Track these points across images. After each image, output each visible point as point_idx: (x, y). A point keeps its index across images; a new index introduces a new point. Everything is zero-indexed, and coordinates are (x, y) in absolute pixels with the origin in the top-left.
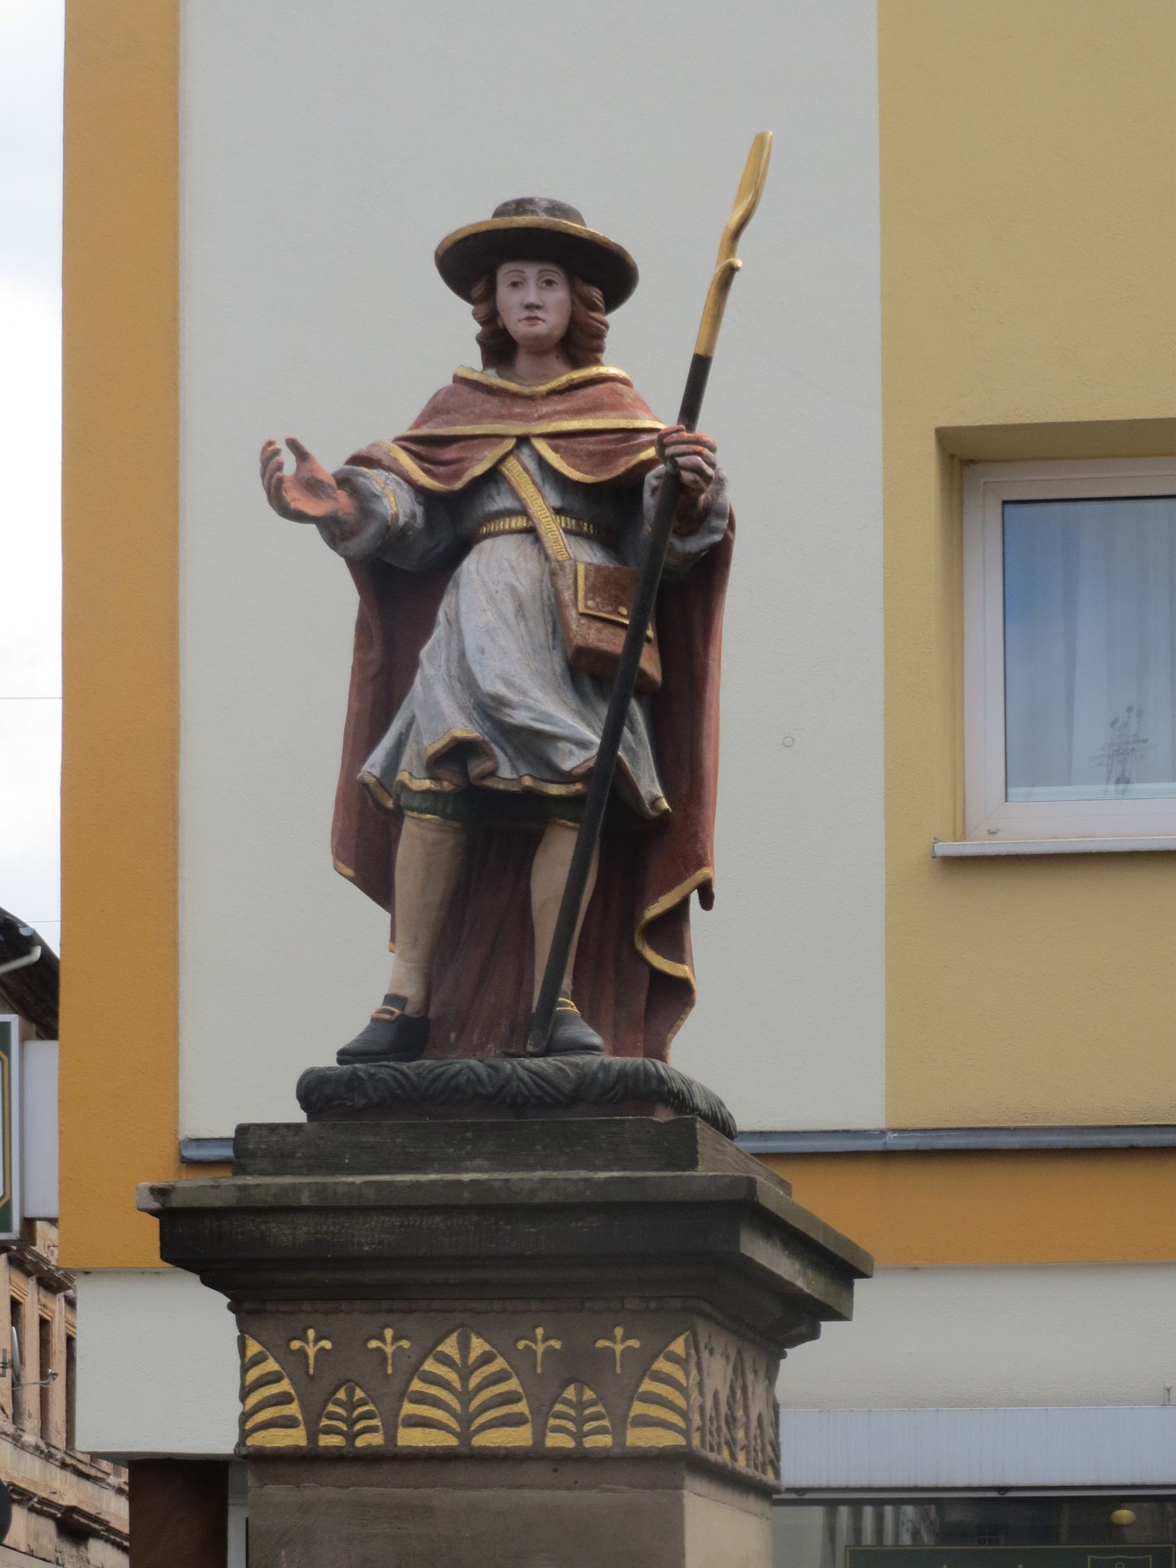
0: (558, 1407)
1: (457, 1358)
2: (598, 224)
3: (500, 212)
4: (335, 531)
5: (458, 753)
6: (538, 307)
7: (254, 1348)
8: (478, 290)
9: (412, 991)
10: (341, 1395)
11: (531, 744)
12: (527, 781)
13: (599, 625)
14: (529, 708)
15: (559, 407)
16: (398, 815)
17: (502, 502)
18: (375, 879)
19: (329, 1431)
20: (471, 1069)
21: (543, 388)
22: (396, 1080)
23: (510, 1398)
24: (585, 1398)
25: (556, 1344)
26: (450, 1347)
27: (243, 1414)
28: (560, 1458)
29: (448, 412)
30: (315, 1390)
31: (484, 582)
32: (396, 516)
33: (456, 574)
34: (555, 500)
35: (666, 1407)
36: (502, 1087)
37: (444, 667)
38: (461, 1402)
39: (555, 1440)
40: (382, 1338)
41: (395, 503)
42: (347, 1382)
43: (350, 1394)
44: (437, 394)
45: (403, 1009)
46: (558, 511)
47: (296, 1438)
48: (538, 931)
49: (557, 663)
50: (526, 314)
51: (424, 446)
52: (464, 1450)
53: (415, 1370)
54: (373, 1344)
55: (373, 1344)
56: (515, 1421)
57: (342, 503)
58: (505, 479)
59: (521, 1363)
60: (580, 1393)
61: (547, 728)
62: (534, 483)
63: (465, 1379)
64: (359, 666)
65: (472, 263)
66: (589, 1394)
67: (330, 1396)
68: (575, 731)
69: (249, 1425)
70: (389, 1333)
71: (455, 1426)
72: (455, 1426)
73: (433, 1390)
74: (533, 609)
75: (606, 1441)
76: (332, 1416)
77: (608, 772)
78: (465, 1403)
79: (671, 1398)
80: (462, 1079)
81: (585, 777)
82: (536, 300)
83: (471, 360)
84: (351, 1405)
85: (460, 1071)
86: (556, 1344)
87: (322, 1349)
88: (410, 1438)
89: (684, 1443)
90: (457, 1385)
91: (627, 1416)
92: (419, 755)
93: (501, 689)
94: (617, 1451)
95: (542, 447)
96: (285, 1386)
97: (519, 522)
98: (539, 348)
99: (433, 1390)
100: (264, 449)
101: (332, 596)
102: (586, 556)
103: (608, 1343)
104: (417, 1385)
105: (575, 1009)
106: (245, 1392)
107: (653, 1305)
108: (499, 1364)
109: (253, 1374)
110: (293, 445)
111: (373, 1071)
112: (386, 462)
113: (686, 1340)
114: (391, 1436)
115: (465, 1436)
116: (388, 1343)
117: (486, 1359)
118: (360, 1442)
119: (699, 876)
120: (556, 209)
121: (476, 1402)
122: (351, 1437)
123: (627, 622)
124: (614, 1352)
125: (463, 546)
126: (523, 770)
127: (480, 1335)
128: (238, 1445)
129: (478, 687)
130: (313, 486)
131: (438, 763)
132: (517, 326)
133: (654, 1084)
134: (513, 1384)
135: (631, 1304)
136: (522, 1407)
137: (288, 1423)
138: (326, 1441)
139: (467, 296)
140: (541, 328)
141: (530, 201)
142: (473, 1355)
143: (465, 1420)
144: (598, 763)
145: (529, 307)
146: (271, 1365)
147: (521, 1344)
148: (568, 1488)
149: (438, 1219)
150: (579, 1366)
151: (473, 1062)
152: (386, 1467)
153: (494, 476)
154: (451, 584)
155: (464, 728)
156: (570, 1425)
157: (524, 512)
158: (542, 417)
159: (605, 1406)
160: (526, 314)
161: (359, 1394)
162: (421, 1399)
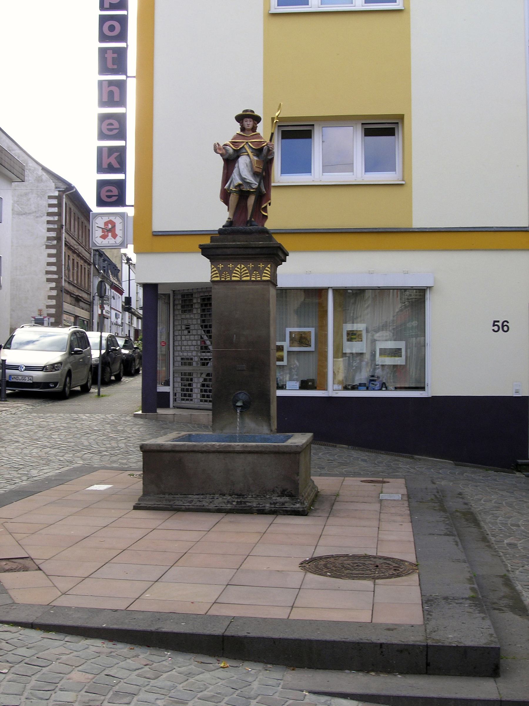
3: (244, 111)
4: (222, 155)
5: (240, 185)
7: (213, 267)
9: (231, 217)
11: (249, 184)
16: (230, 193)
17: (244, 151)
23: (247, 273)
26: (239, 266)
28: (253, 281)
39: (253, 279)
41: (231, 151)
42: (226, 271)
47: (218, 279)
49: (252, 173)
56: (248, 276)
59: (248, 268)
64: (224, 173)
65: (240, 118)
68: (254, 182)
74: (249, 165)
75: (259, 279)
77: (259, 189)
82: (249, 123)
83: (239, 131)
84: (225, 274)
88: (234, 279)
93: (245, 177)
95: (249, 143)
96: (217, 272)
97: (246, 154)
98: (249, 130)
101: (220, 163)
102: (256, 158)
104: (234, 272)
106: (212, 272)
108: (245, 268)
110: (218, 143)
114: (231, 279)
116: (231, 266)
117: (244, 268)
122: (226, 279)
125: (238, 157)
130: (220, 149)
131: (236, 187)
132: (246, 127)
137: (217, 277)
143: (241, 276)
146: (215, 269)
150: (256, 269)
153: (243, 147)
155: (240, 182)
157: (247, 152)
162: (235, 273)
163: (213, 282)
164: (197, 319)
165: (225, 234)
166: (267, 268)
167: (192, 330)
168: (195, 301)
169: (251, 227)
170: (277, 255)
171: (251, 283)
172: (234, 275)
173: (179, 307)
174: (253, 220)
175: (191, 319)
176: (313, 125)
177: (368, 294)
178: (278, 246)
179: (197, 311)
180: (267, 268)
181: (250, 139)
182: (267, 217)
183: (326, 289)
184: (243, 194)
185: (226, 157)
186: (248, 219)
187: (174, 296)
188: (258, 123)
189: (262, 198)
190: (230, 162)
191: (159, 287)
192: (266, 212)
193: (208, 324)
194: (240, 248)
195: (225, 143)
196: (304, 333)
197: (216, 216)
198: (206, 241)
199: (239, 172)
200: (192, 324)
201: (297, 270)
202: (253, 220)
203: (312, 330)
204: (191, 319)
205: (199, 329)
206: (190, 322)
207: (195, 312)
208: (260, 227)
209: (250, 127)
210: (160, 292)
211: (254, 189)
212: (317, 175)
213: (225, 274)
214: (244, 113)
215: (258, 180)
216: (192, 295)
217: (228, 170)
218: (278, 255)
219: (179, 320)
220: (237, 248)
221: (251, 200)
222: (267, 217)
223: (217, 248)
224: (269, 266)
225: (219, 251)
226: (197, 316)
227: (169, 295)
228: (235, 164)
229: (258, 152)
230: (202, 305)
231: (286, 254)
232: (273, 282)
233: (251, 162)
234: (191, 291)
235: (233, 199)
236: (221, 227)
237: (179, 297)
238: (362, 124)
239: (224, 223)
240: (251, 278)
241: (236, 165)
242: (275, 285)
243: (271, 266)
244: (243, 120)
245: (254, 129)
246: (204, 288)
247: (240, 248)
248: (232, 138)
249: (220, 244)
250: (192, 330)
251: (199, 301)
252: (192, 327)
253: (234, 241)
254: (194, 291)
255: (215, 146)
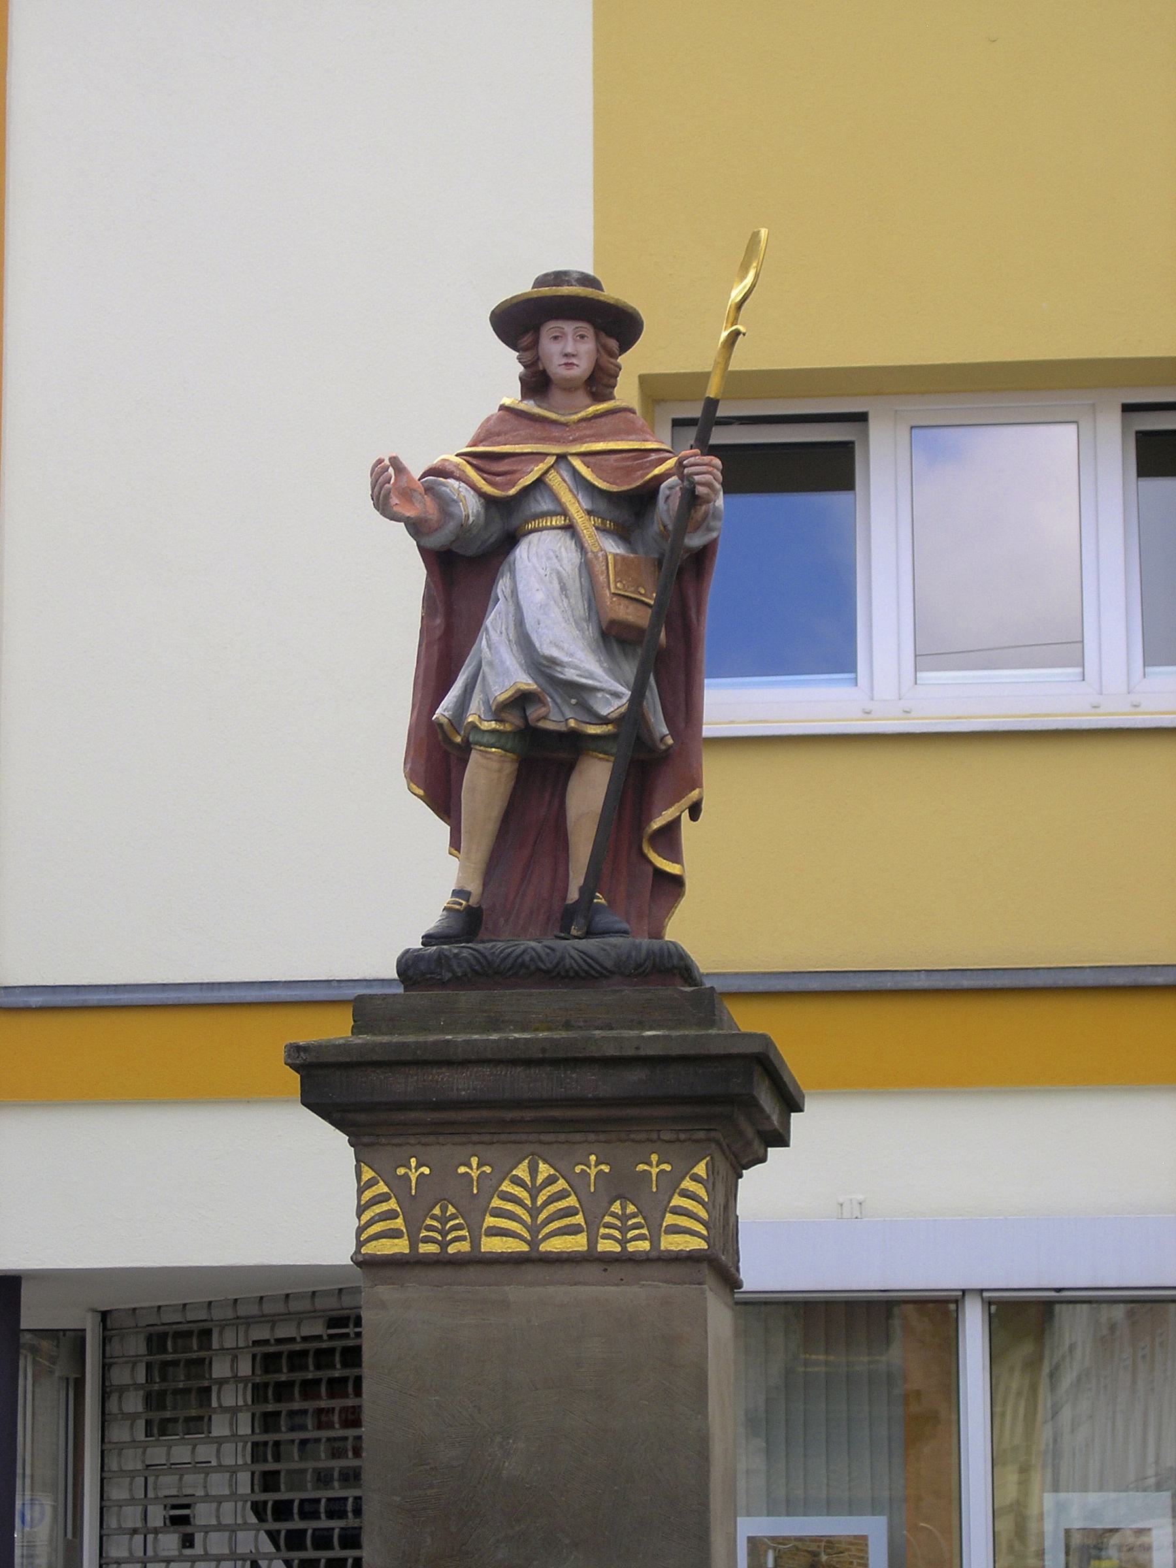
0: (607, 1219)
1: (528, 1180)
2: (613, 291)
3: (541, 282)
4: (416, 528)
5: (522, 700)
6: (573, 355)
7: (368, 1174)
8: (526, 340)
9: (474, 887)
10: (437, 1211)
11: (577, 692)
12: (572, 723)
13: (626, 602)
14: (576, 667)
15: (588, 432)
16: (466, 749)
17: (546, 505)
18: (442, 795)
19: (427, 1240)
20: (533, 949)
21: (576, 417)
22: (475, 958)
23: (569, 1212)
24: (628, 1211)
25: (606, 1168)
26: (522, 1171)
27: (359, 1228)
28: (608, 1260)
29: (499, 434)
30: (415, 1209)
31: (535, 568)
32: (467, 516)
33: (510, 558)
34: (586, 505)
35: (691, 1218)
36: (558, 964)
37: (504, 634)
38: (531, 1216)
39: (605, 1246)
40: (470, 1166)
41: (470, 506)
42: (444, 1201)
43: (444, 1210)
44: (488, 419)
45: (468, 901)
46: (589, 513)
47: (400, 1246)
48: (573, 839)
49: (591, 631)
50: (564, 361)
51: (480, 460)
52: (534, 1255)
53: (495, 1190)
54: (462, 1170)
55: (462, 1170)
56: (574, 1230)
57: (425, 507)
58: (545, 484)
59: (577, 1185)
60: (623, 1208)
61: (590, 682)
62: (571, 491)
63: (534, 1199)
64: (426, 630)
65: (518, 322)
66: (631, 1209)
67: (428, 1212)
68: (610, 687)
69: (364, 1237)
70: (474, 1161)
71: (527, 1235)
72: (527, 1235)
73: (509, 1206)
74: (574, 585)
75: (645, 1246)
76: (430, 1228)
77: (634, 716)
78: (534, 1217)
79: (695, 1211)
80: (527, 958)
81: (619, 721)
82: (570, 348)
83: (512, 395)
84: (444, 1220)
85: (524, 951)
86: (606, 1168)
87: (663, 1171)
88: (491, 1245)
89: (619, 1249)
90: (528, 1202)
91: (661, 1225)
92: (487, 702)
93: (554, 653)
94: (654, 1254)
95: (577, 463)
96: (392, 1204)
97: (559, 521)
98: (569, 387)
99: (509, 1206)
100: (375, 466)
101: (406, 575)
102: (612, 547)
103: (646, 1167)
104: (496, 1202)
105: (603, 901)
106: (361, 1210)
107: (682, 1136)
108: (561, 1184)
109: (368, 1195)
110: (394, 461)
111: (456, 951)
112: (457, 473)
113: (707, 1165)
114: (475, 1244)
115: (533, 1243)
116: (473, 1169)
117: (551, 1181)
118: (451, 1250)
119: (694, 795)
120: (587, 280)
121: (542, 1216)
122: (444, 1245)
123: (652, 602)
124: (650, 1173)
125: (511, 540)
126: (569, 714)
127: (545, 1161)
128: (355, 1253)
129: (535, 650)
130: (407, 494)
131: (500, 711)
132: (556, 367)
133: (675, 961)
134: (572, 1201)
135: (666, 1136)
136: (579, 1219)
137: (394, 1234)
138: (424, 1248)
139: (515, 348)
140: (575, 372)
141: (565, 273)
142: (540, 1179)
143: (534, 1230)
144: (629, 708)
145: (566, 355)
146: (382, 1188)
147: (578, 1169)
148: (617, 1285)
149: (519, 1069)
150: (623, 1185)
151: (533, 944)
152: (472, 1269)
153: (540, 482)
154: (505, 567)
155: (526, 682)
156: (617, 1234)
157: (564, 513)
158: (574, 441)
159: (644, 1218)
160: (564, 361)
161: (451, 1210)
162: (499, 1213)
163: (365, 1263)
164: (233, 1471)
165: (443, 984)
166: (688, 1184)
167: (207, 1530)
168: (220, 1369)
169: (583, 944)
170: (733, 1101)
171: (594, 1271)
172: (490, 1221)
173: (134, 1403)
174: (600, 899)
175: (203, 1468)
176: (862, 418)
177: (1074, 1329)
178: (755, 1048)
179: (234, 1423)
180: (688, 1184)
181: (581, 440)
182: (677, 882)
183: (939, 1311)
184: (542, 754)
185: (436, 541)
186: (573, 895)
187: (105, 1341)
188: (624, 348)
189: (654, 765)
190: (463, 571)
191: (27, 1294)
192: (676, 858)
193: (297, 1496)
194: (528, 1063)
195: (435, 461)
196: (830, 1543)
197: (376, 887)
198: (334, 1029)
199: (520, 623)
200: (207, 1498)
201: (851, 1192)
202: (600, 899)
203: (873, 1529)
204: (203, 1468)
205: (245, 1526)
206: (193, 1484)
207: (220, 1427)
208: (645, 942)
209: (582, 368)
210: (30, 1319)
211: (605, 721)
212: (888, 683)
213: (444, 1220)
214: (546, 291)
215: (630, 670)
216: (206, 1334)
217: (450, 613)
218: (750, 1104)
219: (132, 1475)
220: (514, 1062)
221: (590, 789)
222: (677, 882)
223: (372, 1074)
224: (701, 1169)
225: (404, 1084)
226: (233, 1455)
227: (79, 1337)
228: (493, 582)
229: (628, 510)
230: (259, 1392)
231: (792, 1103)
232: (718, 1265)
233: (587, 567)
234: (177, 1317)
235: (485, 780)
236: (418, 945)
237: (136, 1346)
238: (1127, 408)
239: (431, 917)
240: (592, 1243)
241: (502, 586)
242: (729, 1280)
243: (711, 1169)
244: (537, 330)
245: (599, 383)
246: (273, 1298)
247: (528, 1063)
248: (469, 438)
249: (411, 1039)
250: (207, 1530)
251: (245, 1369)
252: (203, 1514)
253: (494, 1024)
254: (217, 1314)
255: (378, 473)
